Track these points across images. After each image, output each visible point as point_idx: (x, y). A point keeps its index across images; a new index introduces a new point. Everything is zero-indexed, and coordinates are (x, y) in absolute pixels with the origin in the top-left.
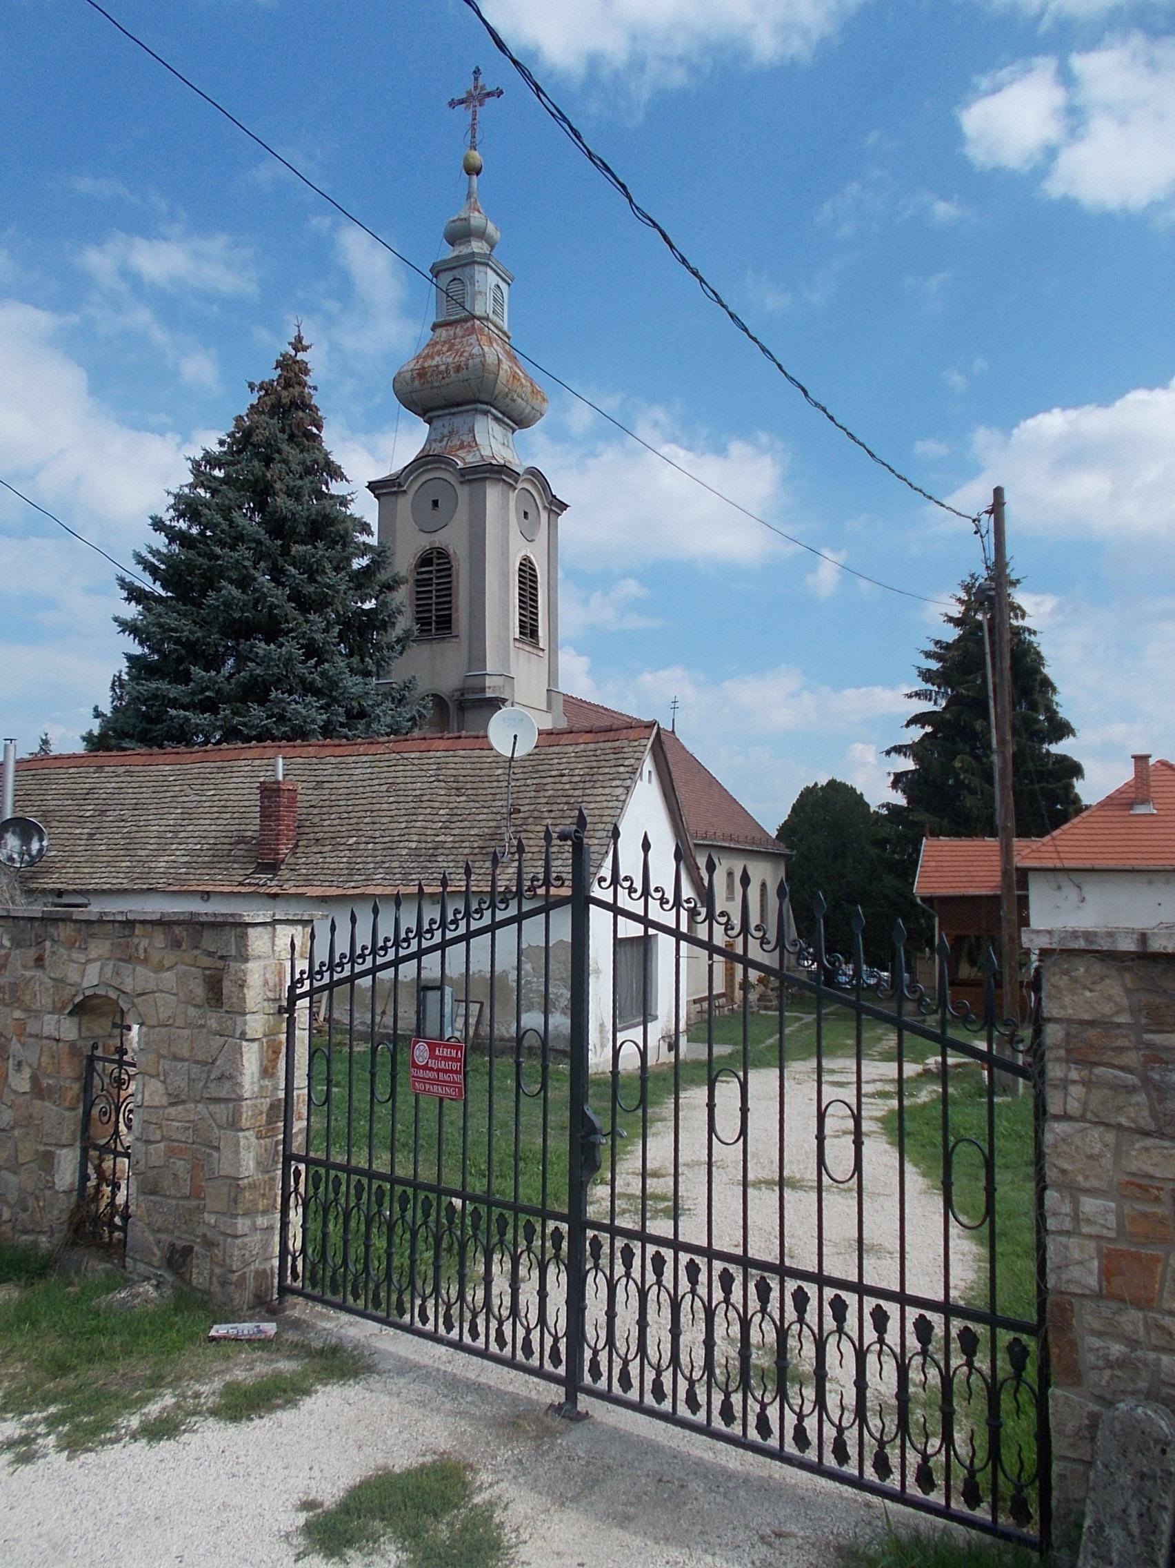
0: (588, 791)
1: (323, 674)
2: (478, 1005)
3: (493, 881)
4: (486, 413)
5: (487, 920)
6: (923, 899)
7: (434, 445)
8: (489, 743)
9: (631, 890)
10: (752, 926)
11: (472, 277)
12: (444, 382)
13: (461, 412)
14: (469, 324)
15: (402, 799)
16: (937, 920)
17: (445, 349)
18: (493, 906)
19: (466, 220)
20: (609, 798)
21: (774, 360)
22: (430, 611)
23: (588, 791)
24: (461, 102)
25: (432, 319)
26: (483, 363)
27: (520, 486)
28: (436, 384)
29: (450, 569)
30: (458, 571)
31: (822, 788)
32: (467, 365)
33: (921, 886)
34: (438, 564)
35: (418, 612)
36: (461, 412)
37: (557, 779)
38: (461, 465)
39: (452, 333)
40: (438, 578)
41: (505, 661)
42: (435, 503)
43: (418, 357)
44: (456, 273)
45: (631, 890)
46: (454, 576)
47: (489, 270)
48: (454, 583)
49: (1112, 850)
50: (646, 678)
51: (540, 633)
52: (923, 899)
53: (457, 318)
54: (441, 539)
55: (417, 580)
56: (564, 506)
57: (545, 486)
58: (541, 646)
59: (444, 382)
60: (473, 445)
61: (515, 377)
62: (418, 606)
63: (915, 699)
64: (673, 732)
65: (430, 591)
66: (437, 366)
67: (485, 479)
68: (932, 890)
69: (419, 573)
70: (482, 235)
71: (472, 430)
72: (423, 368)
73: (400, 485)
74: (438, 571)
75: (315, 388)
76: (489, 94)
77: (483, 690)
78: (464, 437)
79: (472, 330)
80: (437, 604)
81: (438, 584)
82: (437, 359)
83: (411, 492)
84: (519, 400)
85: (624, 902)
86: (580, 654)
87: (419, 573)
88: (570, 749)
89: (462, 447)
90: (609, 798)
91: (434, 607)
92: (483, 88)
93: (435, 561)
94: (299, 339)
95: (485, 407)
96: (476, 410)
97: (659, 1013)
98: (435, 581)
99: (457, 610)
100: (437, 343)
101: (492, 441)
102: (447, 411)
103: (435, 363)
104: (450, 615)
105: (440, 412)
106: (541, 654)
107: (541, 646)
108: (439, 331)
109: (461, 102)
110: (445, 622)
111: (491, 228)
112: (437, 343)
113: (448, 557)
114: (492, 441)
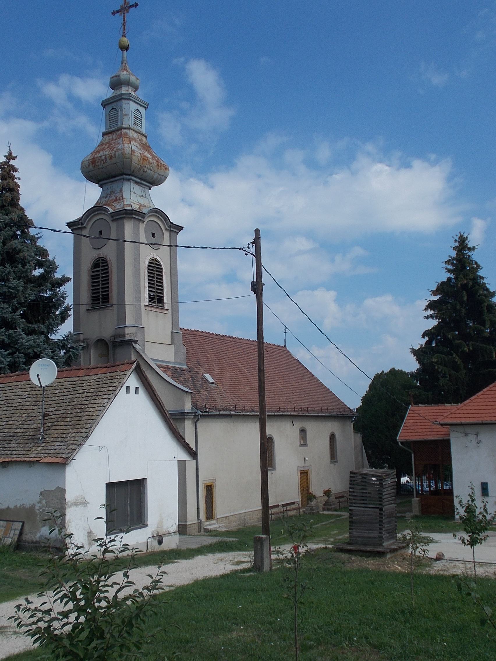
0: (92, 402)
1: (9, 336)
2: (21, 524)
4: (129, 180)
6: (402, 443)
7: (103, 200)
8: (30, 378)
11: (121, 107)
12: (104, 165)
13: (116, 181)
14: (120, 132)
15: (9, 408)
16: (413, 455)
17: (106, 147)
19: (118, 76)
20: (99, 405)
22: (99, 292)
23: (92, 402)
24: (118, 12)
25: (103, 130)
26: (123, 154)
27: (147, 220)
28: (101, 167)
29: (108, 269)
31: (387, 374)
32: (115, 155)
33: (403, 435)
35: (93, 293)
36: (116, 181)
38: (111, 210)
39: (111, 137)
40: (102, 274)
41: (138, 318)
43: (93, 152)
44: (114, 105)
47: (131, 102)
48: (110, 276)
49: (474, 412)
50: (369, 302)
51: (165, 300)
52: (402, 443)
53: (114, 130)
55: (92, 276)
56: (180, 228)
57: (165, 218)
58: (166, 307)
59: (104, 165)
60: (120, 199)
61: (145, 159)
62: (93, 290)
63: (430, 319)
64: (285, 346)
65: (99, 282)
66: (101, 157)
67: (124, 218)
68: (407, 438)
69: (93, 272)
70: (128, 83)
71: (121, 190)
72: (94, 158)
73: (82, 224)
74: (102, 270)
75: (19, 179)
76: (131, 6)
77: (124, 336)
78: (117, 195)
79: (121, 136)
80: (102, 288)
81: (102, 277)
82: (101, 152)
83: (89, 227)
84: (149, 171)
86: (328, 290)
87: (93, 272)
88: (93, 377)
89: (116, 200)
90: (99, 405)
91: (100, 290)
92: (128, 3)
93: (101, 265)
94: (10, 154)
95: (128, 177)
96: (123, 179)
97: (148, 523)
98: (101, 276)
99: (112, 291)
100: (103, 144)
101: (132, 196)
102: (108, 181)
103: (100, 155)
104: (108, 294)
105: (105, 182)
106: (166, 312)
107: (166, 307)
108: (105, 137)
109: (118, 12)
111: (133, 79)
112: (103, 144)
113: (106, 262)
114: (132, 196)
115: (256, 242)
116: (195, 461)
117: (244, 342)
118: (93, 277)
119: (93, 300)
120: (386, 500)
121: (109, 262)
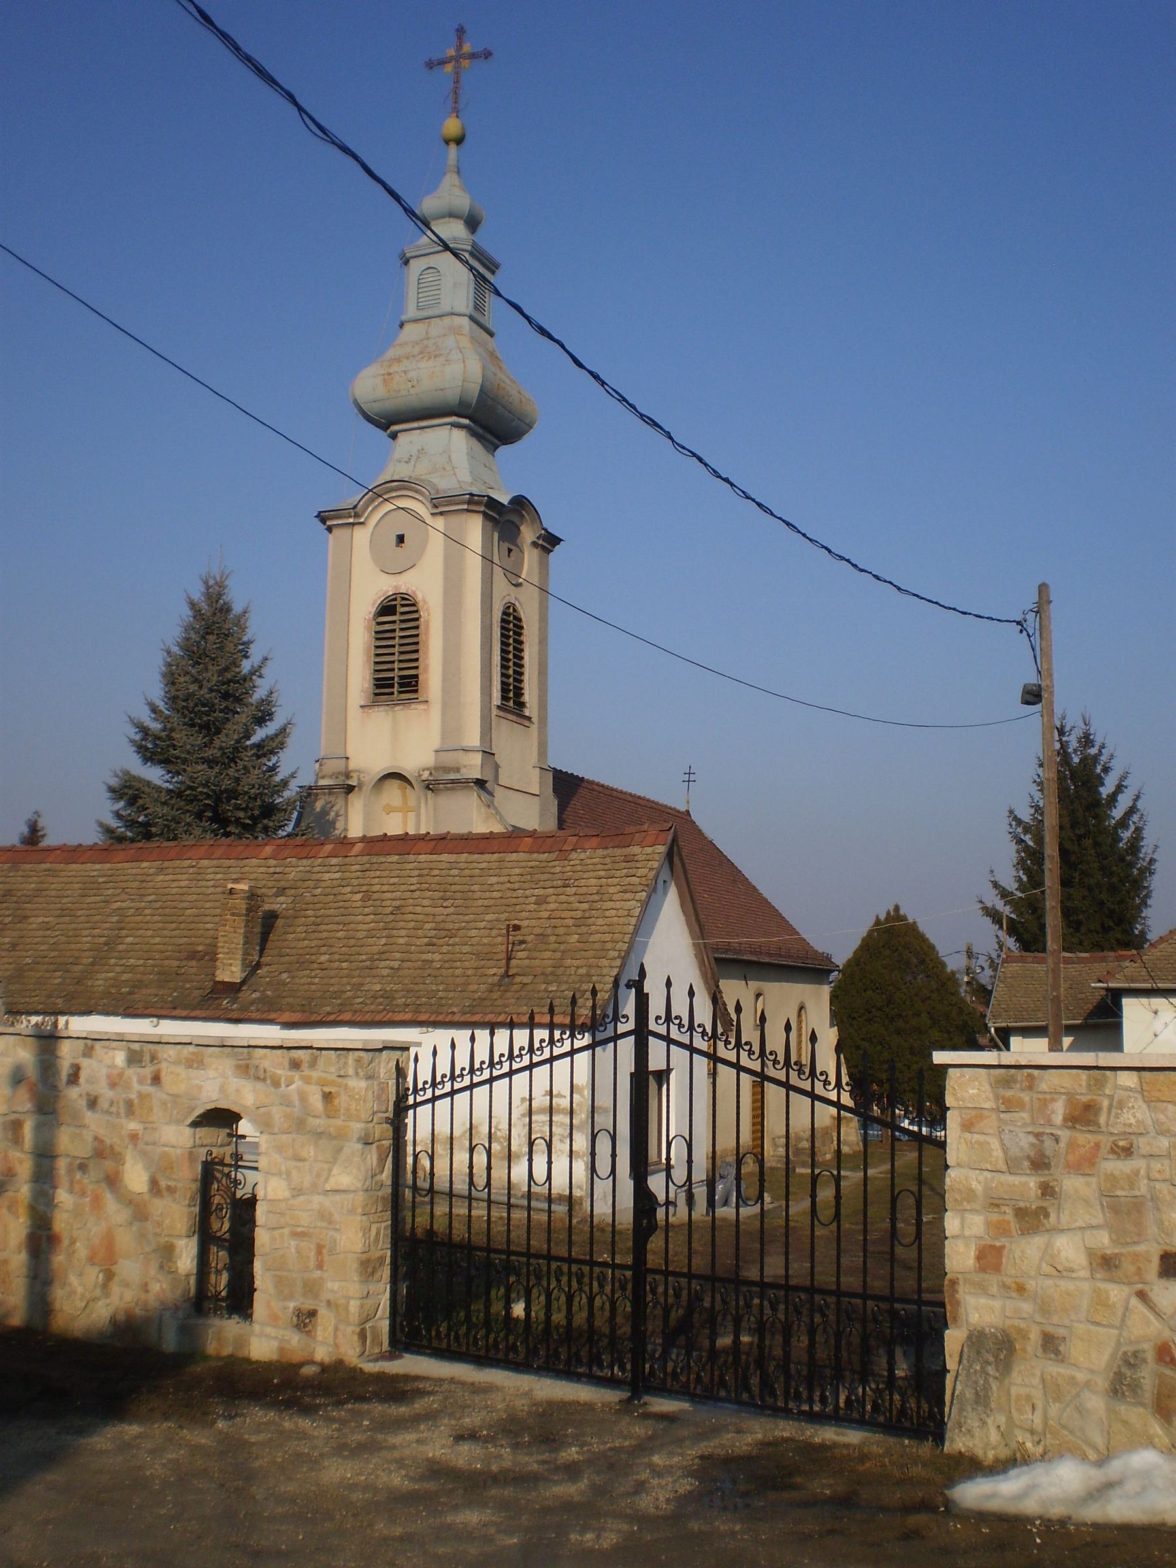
3: (573, 1014)
5: (567, 1047)
9: (680, 1026)
10: (793, 1060)
18: (572, 1036)
21: (799, 532)
30: (427, 623)
34: (402, 613)
37: (561, 890)
42: (401, 539)
45: (680, 1026)
46: (422, 627)
54: (406, 583)
73: (357, 515)
74: (402, 621)
85: (675, 1034)
87: (379, 624)
93: (401, 609)
99: (426, 670)
102: (415, 425)
104: (416, 676)
110: (409, 685)
115: (1041, 608)
116: (1126, 1002)
117: (623, 796)
118: (380, 635)
119: (378, 686)
120: (540, 1173)
121: (420, 605)
